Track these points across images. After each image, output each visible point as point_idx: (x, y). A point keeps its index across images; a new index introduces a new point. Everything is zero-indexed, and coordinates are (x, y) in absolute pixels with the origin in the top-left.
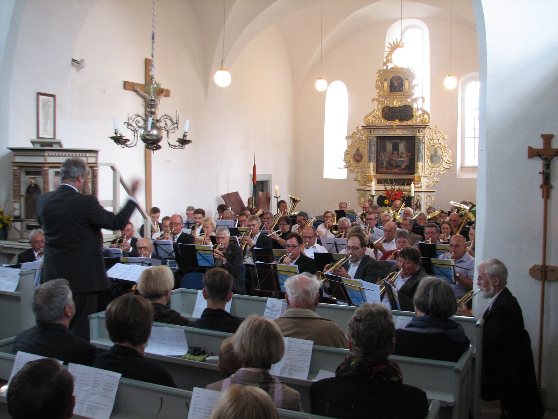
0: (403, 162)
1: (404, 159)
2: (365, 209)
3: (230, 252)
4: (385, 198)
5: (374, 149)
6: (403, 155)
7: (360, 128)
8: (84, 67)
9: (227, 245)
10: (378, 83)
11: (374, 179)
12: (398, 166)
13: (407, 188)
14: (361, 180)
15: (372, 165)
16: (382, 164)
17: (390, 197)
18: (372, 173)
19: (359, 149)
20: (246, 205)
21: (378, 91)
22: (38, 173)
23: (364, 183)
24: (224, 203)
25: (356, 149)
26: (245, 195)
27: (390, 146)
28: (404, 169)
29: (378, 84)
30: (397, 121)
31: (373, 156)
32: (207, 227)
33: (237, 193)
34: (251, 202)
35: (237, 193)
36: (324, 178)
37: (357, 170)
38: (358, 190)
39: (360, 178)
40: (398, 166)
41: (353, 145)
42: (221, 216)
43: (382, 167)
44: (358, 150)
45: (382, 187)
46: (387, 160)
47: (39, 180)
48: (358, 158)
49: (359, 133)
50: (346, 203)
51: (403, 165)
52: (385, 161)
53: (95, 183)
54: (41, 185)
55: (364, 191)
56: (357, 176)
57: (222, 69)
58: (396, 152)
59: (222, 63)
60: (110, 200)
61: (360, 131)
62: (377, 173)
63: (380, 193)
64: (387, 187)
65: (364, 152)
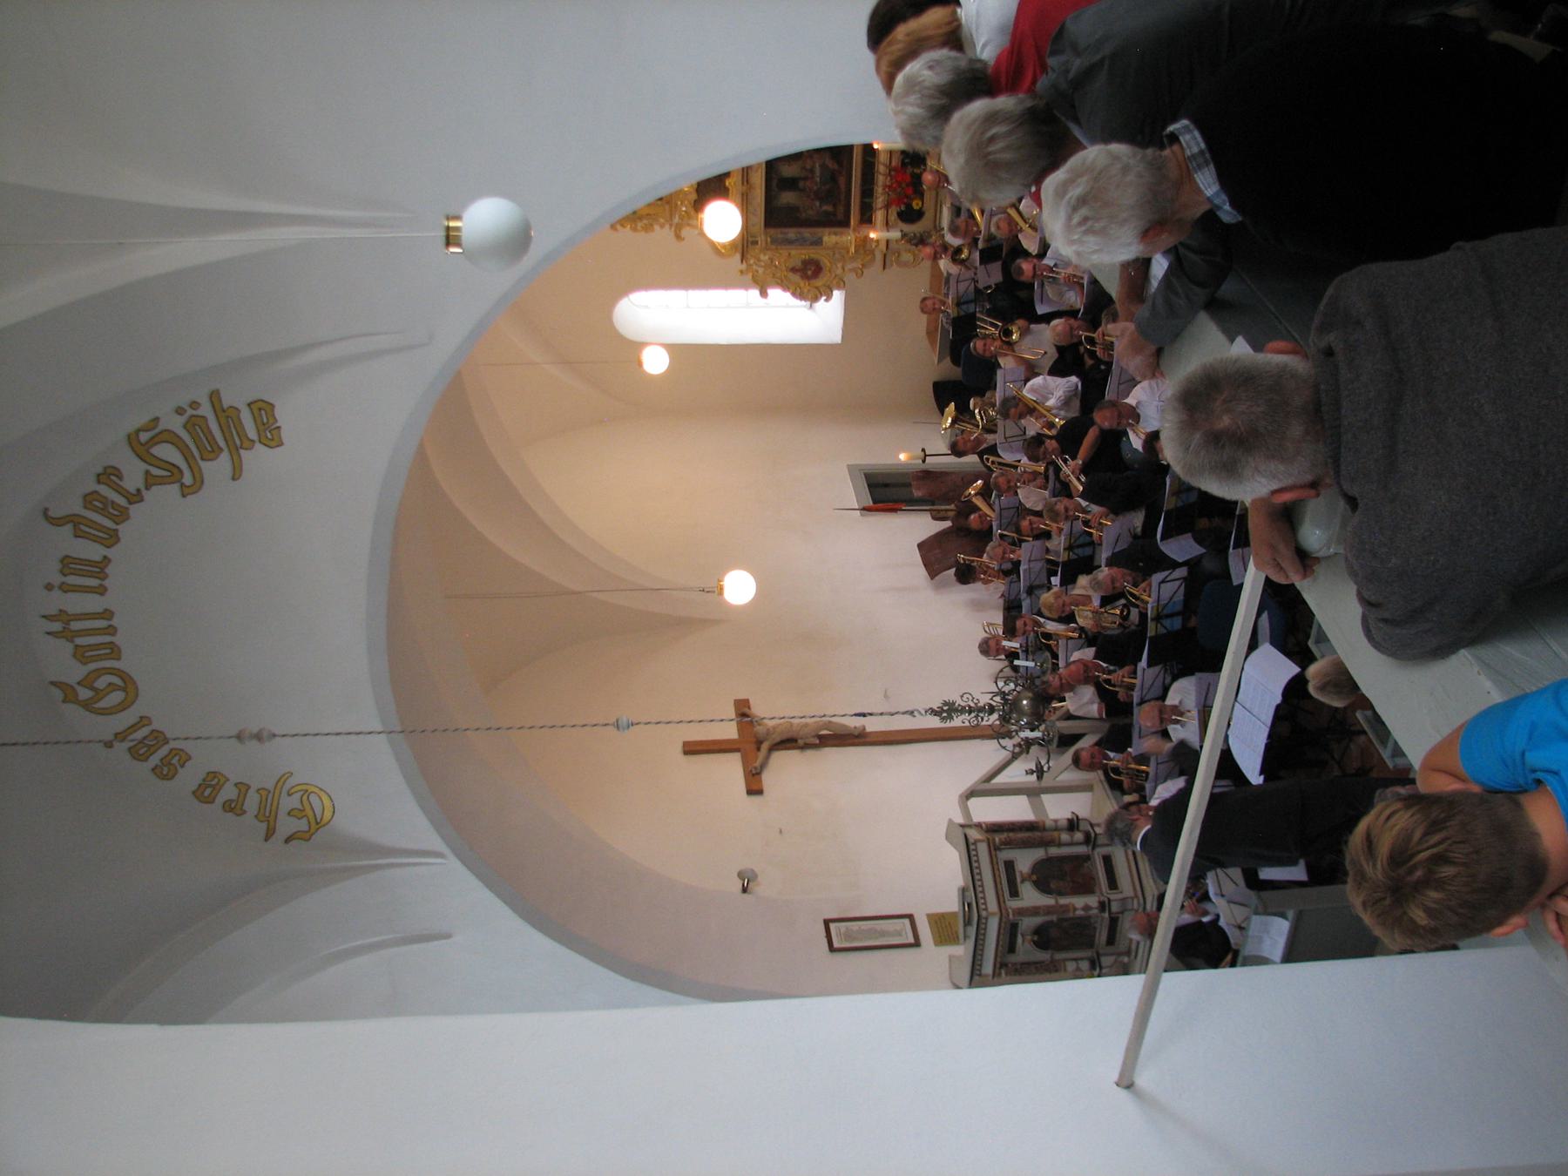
0: (823, 166)
1: (817, 165)
2: (939, 256)
3: (1141, 564)
4: (909, 206)
5: (792, 233)
6: (808, 167)
7: (744, 266)
8: (753, 871)
9: (1126, 571)
10: (639, 228)
11: (862, 234)
12: (833, 178)
13: (883, 158)
14: (862, 260)
15: (830, 238)
16: (827, 213)
17: (907, 197)
18: (849, 238)
19: (790, 267)
20: (948, 524)
21: (667, 226)
22: (1014, 927)
23: (868, 255)
24: (954, 570)
25: (791, 275)
26: (921, 526)
27: (788, 198)
28: (840, 164)
29: (642, 227)
30: (730, 183)
31: (807, 232)
32: (1064, 605)
33: (920, 546)
34: (942, 514)
35: (920, 546)
36: (840, 342)
37: (839, 271)
38: (884, 268)
39: (858, 264)
40: (833, 178)
41: (782, 281)
42: (982, 576)
43: (834, 214)
44: (794, 270)
45: (879, 216)
46: (818, 204)
47: (1028, 924)
48: (810, 269)
49: (754, 267)
50: (919, 300)
51: (830, 165)
52: (820, 206)
53: (1011, 826)
54: (1037, 921)
55: (889, 254)
56: (850, 270)
57: (721, 589)
58: (801, 184)
59: (706, 590)
60: (1030, 802)
61: (749, 266)
62: (845, 223)
63: (893, 216)
64: (879, 205)
65: (798, 255)
